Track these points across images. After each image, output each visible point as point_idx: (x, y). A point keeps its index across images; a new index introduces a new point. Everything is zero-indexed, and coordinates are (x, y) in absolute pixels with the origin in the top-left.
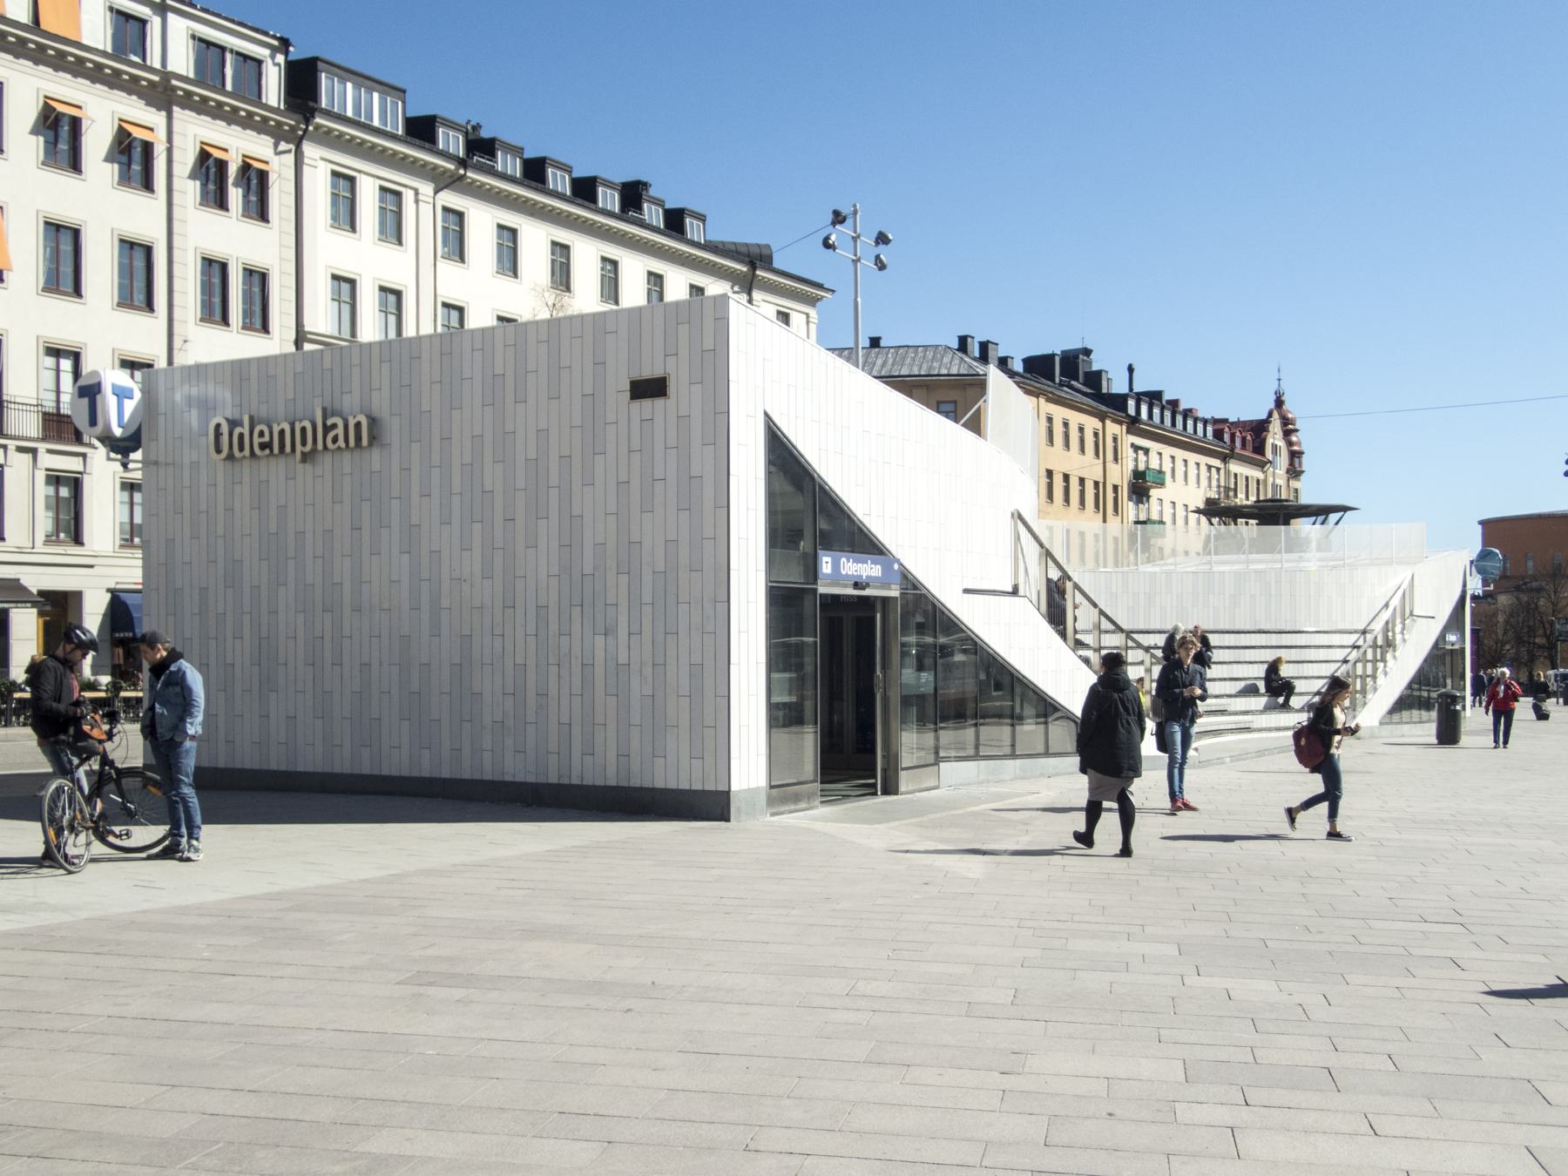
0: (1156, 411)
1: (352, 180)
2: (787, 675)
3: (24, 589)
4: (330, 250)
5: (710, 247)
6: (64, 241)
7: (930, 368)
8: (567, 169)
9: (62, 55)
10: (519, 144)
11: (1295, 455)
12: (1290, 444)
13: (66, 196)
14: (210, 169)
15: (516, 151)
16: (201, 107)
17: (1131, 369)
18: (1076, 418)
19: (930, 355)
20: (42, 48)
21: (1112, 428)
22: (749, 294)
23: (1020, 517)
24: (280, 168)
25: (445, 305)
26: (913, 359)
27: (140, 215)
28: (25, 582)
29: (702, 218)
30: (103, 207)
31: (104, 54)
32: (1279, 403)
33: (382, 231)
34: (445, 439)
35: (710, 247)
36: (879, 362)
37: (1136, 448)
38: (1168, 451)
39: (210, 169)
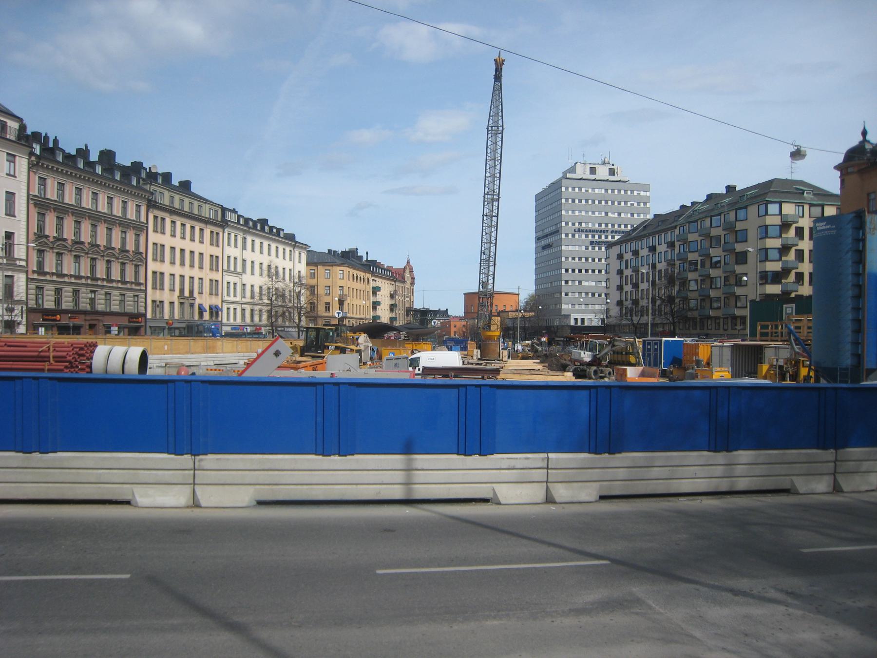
11: (413, 279)
38: (380, 280)
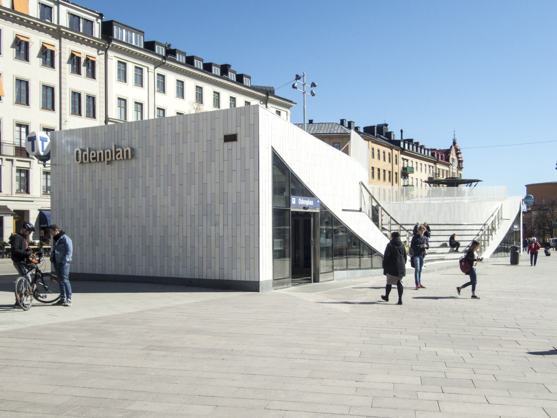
0: (411, 146)
1: (125, 64)
2: (280, 240)
3: (9, 209)
4: (117, 89)
5: (252, 88)
6: (23, 86)
7: (330, 131)
8: (201, 60)
9: (22, 19)
10: (185, 51)
11: (460, 162)
12: (458, 158)
13: (23, 70)
14: (75, 60)
15: (183, 54)
16: (72, 38)
17: (402, 131)
18: (382, 149)
19: (330, 126)
20: (15, 17)
21: (395, 152)
22: (266, 104)
23: (362, 184)
24: (99, 60)
25: (158, 108)
26: (324, 128)
27: (50, 77)
28: (9, 207)
29: (249, 78)
30: (37, 73)
31: (37, 19)
32: (454, 143)
33: (136, 82)
34: (158, 156)
35: (252, 88)
36: (312, 129)
37: (404, 159)
38: (415, 160)
39: (75, 60)
